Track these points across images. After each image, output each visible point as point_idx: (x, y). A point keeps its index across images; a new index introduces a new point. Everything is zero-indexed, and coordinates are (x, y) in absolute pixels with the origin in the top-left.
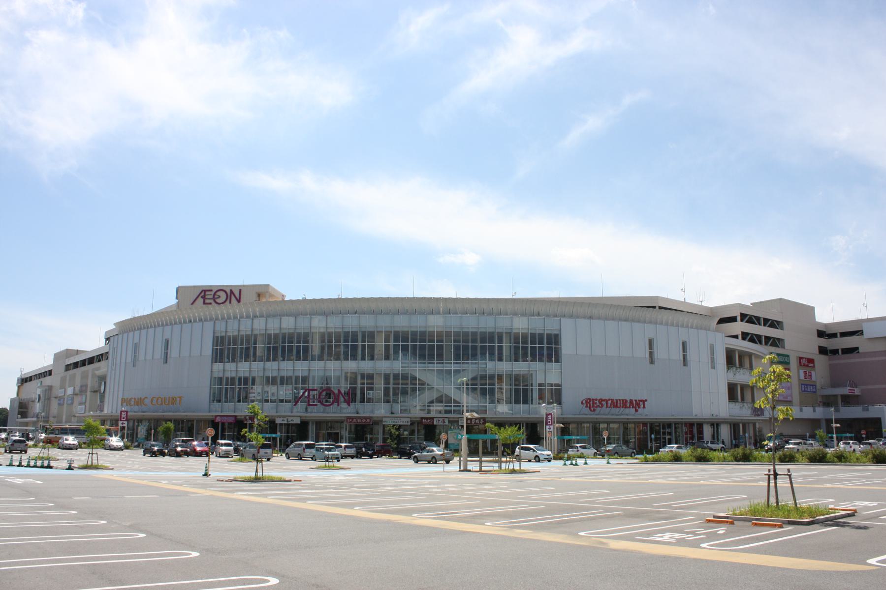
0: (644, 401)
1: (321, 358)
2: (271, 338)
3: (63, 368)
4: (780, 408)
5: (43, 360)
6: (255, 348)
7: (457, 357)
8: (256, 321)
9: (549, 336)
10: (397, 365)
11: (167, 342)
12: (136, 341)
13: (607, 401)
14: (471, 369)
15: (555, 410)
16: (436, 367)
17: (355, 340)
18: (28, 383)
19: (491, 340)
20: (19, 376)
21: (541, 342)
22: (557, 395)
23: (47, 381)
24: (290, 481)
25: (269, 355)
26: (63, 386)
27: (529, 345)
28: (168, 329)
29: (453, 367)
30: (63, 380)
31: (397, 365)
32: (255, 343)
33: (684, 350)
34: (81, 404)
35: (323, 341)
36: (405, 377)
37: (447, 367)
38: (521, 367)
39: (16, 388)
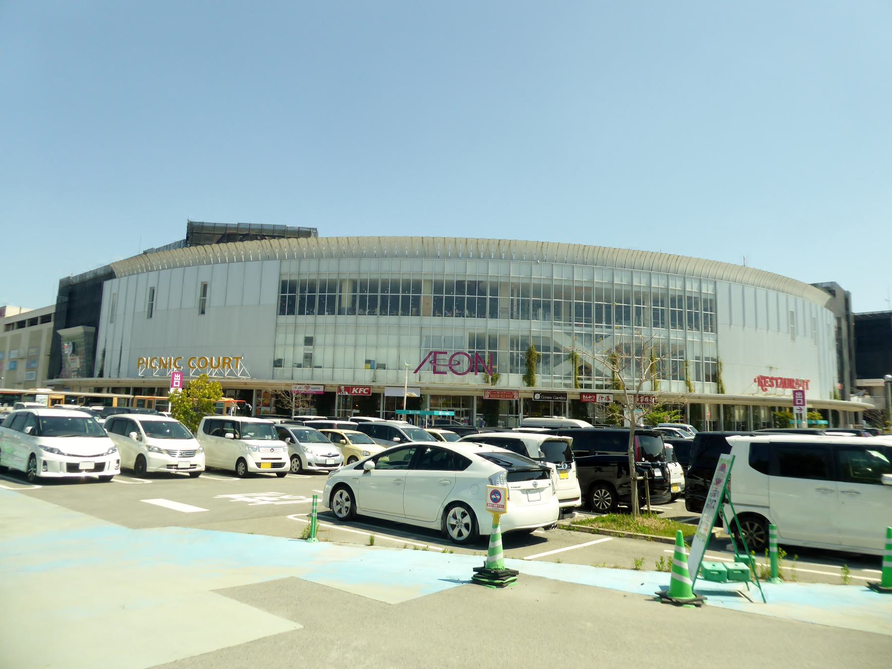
1: (352, 311)
2: (522, 290)
4: (78, 361)
8: (286, 264)
11: (153, 291)
12: (115, 291)
13: (776, 379)
14: (621, 334)
17: (312, 289)
24: (102, 455)
27: (379, 294)
32: (340, 291)
33: (204, 293)
35: (355, 291)
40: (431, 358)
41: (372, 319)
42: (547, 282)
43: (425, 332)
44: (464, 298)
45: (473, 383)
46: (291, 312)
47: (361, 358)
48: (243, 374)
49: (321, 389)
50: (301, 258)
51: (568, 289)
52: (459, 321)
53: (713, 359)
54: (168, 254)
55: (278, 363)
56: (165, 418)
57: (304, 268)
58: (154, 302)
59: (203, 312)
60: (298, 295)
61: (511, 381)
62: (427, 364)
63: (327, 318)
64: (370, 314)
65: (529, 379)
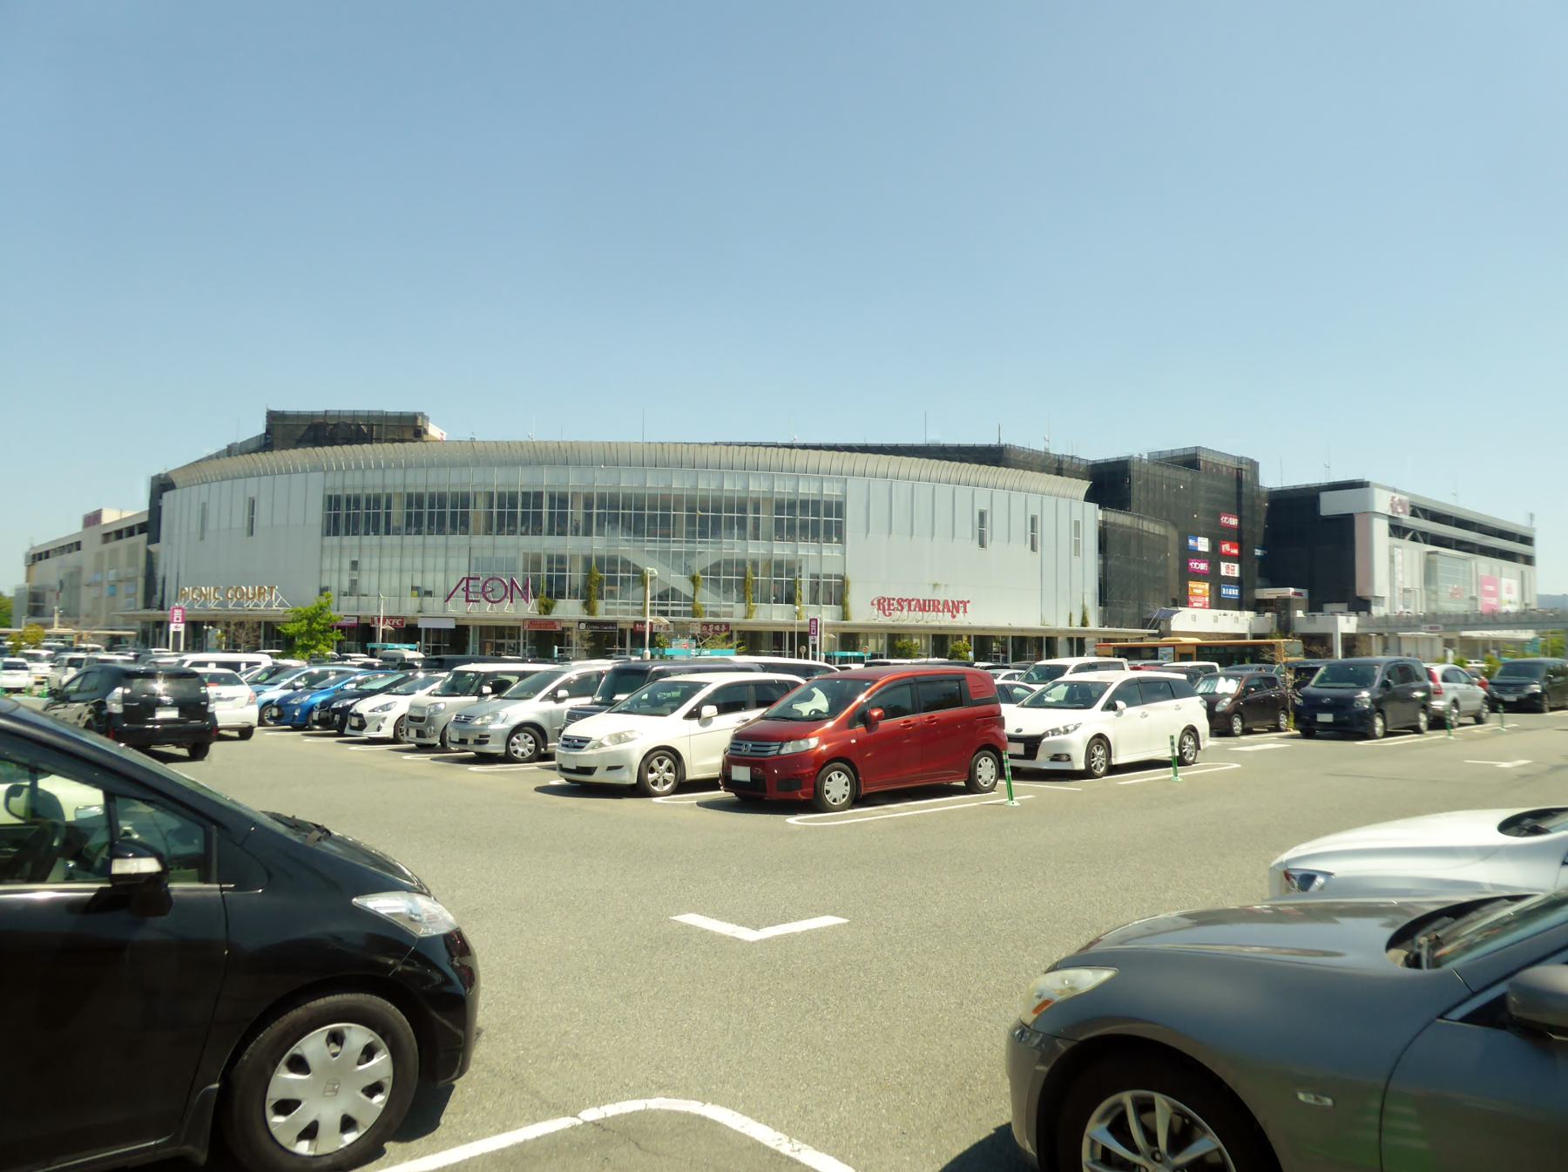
0: (965, 603)
2: (414, 500)
3: (99, 539)
5: (70, 526)
6: (388, 516)
7: (691, 534)
9: (828, 505)
10: (597, 545)
13: (910, 602)
14: (709, 552)
15: (827, 615)
16: (657, 547)
18: (44, 562)
19: (743, 509)
20: (27, 548)
21: (420, 505)
22: (837, 592)
23: (71, 558)
25: (408, 524)
26: (99, 569)
28: (252, 482)
29: (684, 548)
30: (99, 555)
31: (597, 545)
32: (388, 507)
34: (128, 596)
36: (613, 561)
37: (674, 547)
38: (782, 550)
39: (24, 569)
40: (464, 585)
41: (441, 539)
42: (717, 494)
43: (475, 553)
44: (518, 513)
45: (524, 610)
46: (336, 533)
47: (407, 582)
48: (281, 604)
49: (355, 621)
50: (408, 466)
51: (816, 503)
52: (511, 540)
53: (837, 577)
54: (215, 462)
55: (323, 590)
56: (376, 662)
57: (348, 482)
58: (987, 530)
59: (251, 533)
60: (426, 510)
61: (568, 610)
62: (460, 592)
63: (373, 539)
64: (534, 534)
65: (547, 609)
